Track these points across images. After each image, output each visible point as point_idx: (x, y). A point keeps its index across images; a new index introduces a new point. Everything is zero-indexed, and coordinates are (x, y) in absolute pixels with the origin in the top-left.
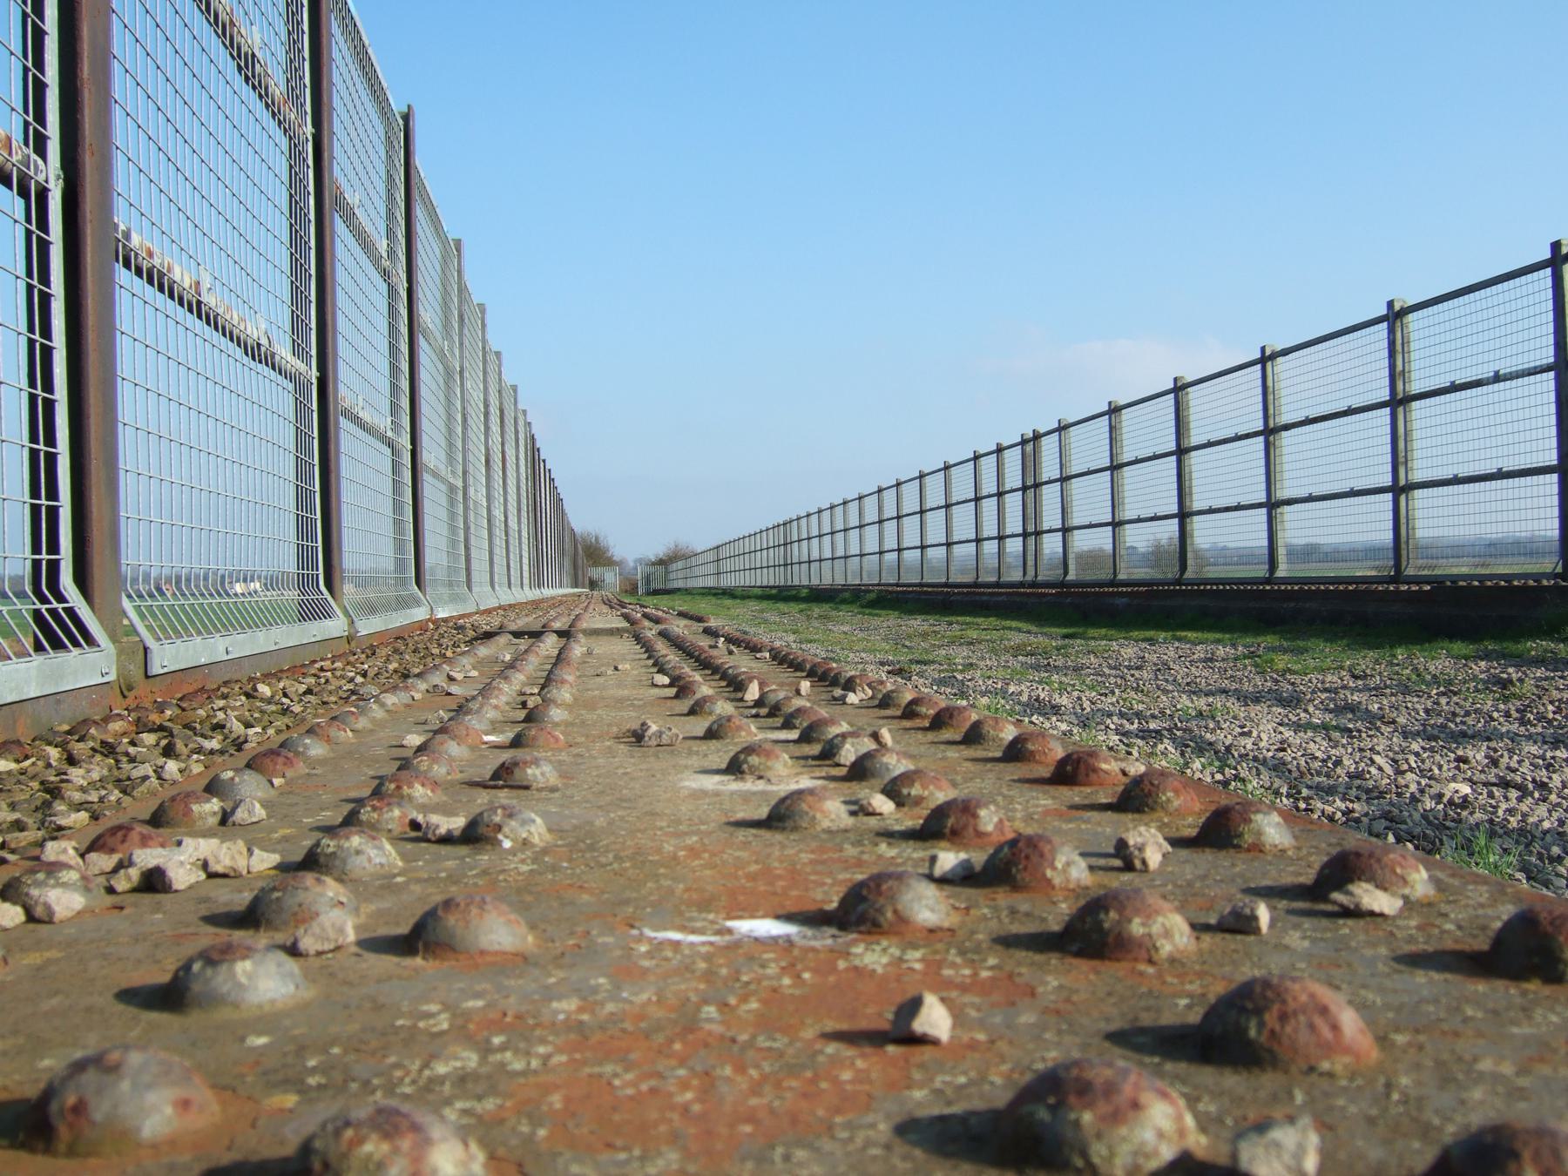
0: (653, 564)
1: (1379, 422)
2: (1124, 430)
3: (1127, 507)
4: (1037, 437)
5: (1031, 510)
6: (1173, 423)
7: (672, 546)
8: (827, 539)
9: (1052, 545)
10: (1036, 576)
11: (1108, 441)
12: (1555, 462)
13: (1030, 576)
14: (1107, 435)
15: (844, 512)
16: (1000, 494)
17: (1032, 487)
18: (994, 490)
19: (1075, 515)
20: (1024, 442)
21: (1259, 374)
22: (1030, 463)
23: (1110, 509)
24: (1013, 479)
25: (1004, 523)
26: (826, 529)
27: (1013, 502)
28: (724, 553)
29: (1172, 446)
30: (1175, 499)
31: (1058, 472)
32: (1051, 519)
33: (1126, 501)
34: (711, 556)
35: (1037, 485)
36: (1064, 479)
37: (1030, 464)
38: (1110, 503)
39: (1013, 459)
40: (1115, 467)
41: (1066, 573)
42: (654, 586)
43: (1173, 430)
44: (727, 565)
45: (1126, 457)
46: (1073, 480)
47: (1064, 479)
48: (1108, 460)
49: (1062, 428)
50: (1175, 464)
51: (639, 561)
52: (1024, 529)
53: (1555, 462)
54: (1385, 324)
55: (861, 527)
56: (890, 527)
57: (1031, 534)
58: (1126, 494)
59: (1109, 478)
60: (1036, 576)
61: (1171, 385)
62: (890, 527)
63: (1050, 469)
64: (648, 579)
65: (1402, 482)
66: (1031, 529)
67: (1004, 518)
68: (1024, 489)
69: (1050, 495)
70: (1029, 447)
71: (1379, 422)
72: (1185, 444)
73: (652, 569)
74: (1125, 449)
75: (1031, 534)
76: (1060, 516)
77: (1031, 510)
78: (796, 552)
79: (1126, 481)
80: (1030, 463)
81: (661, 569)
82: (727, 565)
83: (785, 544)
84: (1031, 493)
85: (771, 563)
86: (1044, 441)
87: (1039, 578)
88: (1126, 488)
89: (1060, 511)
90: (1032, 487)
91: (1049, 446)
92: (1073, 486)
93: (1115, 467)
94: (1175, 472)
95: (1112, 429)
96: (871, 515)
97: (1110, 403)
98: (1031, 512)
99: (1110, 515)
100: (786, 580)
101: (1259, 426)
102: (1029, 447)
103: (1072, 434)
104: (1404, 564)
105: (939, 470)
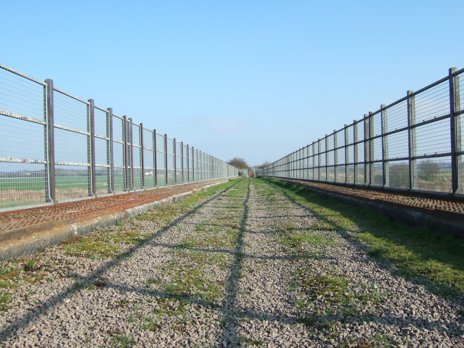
0: (259, 168)
1: (342, 150)
2: (416, 106)
3: (417, 149)
4: (371, 115)
5: (368, 151)
6: (363, 131)
7: (265, 162)
8: (317, 157)
9: (377, 169)
10: (370, 183)
11: (407, 113)
12: (450, 152)
13: (367, 183)
14: (407, 110)
15: (303, 152)
16: (355, 144)
17: (369, 140)
18: (352, 142)
19: (389, 153)
20: (365, 118)
21: (344, 131)
22: (368, 128)
23: (408, 150)
24: (361, 137)
25: (357, 157)
26: (311, 154)
27: (361, 147)
28: (294, 157)
29: (448, 112)
30: (450, 144)
31: (381, 132)
32: (377, 155)
33: (417, 146)
34: (285, 161)
35: (371, 139)
36: (384, 135)
37: (368, 129)
38: (408, 147)
39: (360, 126)
40: (411, 127)
41: (384, 183)
42: (259, 175)
43: (449, 102)
44: (292, 166)
45: (417, 121)
46: (388, 136)
47: (384, 135)
48: (407, 123)
49: (383, 109)
50: (449, 123)
51: (255, 167)
52: (365, 160)
53: (450, 152)
54: (448, 80)
55: (319, 154)
56: (331, 154)
57: (368, 163)
58: (417, 142)
59: (407, 134)
60: (370, 183)
61: (447, 74)
62: (331, 154)
63: (377, 131)
64: (257, 173)
65: (412, 156)
66: (368, 160)
67: (357, 155)
68: (365, 141)
69: (377, 143)
70: (367, 121)
71: (342, 150)
72: (457, 109)
73: (258, 170)
74: (416, 117)
75: (368, 163)
76: (381, 154)
77: (368, 151)
78: (302, 164)
79: (417, 135)
80: (368, 128)
81: (261, 170)
82: (292, 166)
83: (288, 163)
84: (368, 143)
85: (298, 168)
86: (375, 117)
87: (372, 184)
88: (417, 138)
89: (381, 151)
90: (369, 140)
91: (377, 119)
92: (329, 154)
93: (411, 127)
94: (449, 127)
95: (409, 106)
96: (341, 143)
97: (408, 92)
98: (369, 152)
99: (381, 157)
100: (288, 176)
101: (406, 125)
102: (367, 121)
103: (337, 135)
104: (412, 185)
105: (342, 129)
